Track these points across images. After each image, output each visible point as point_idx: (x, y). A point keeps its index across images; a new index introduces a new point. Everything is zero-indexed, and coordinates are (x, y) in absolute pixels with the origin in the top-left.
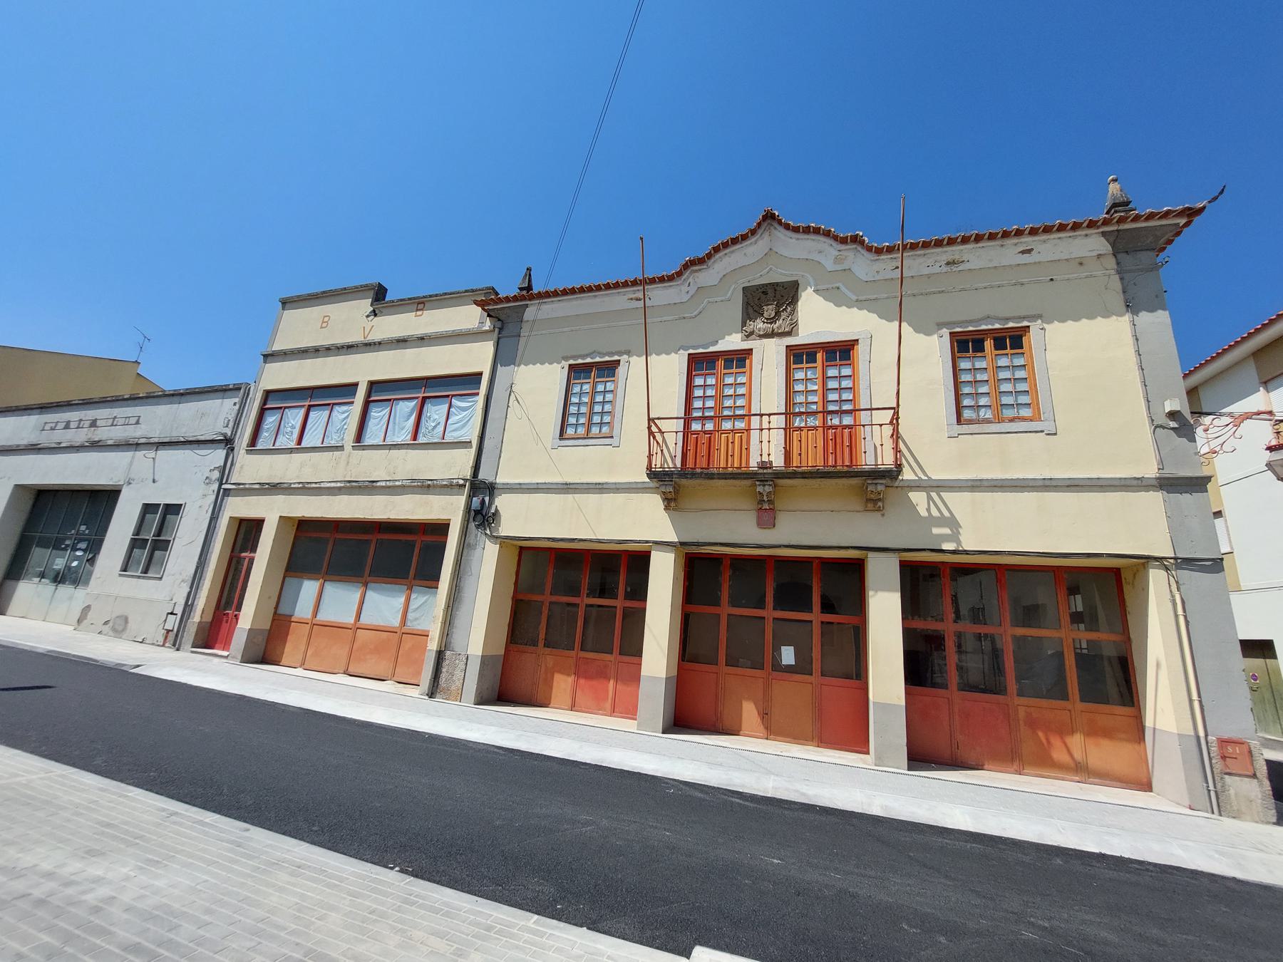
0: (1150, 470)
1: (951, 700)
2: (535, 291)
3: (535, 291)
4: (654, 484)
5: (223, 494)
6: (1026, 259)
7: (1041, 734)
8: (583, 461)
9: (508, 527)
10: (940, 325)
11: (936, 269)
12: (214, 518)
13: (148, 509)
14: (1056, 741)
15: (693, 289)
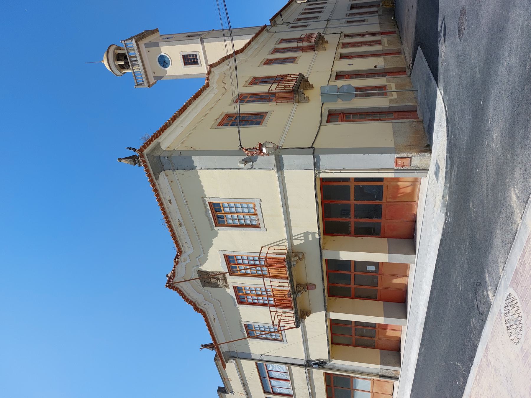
2: (212, 342)
3: (212, 342)
4: (301, 325)
6: (173, 201)
7: (399, 195)
9: (325, 356)
10: (212, 229)
11: (184, 229)
14: (402, 191)
15: (206, 303)
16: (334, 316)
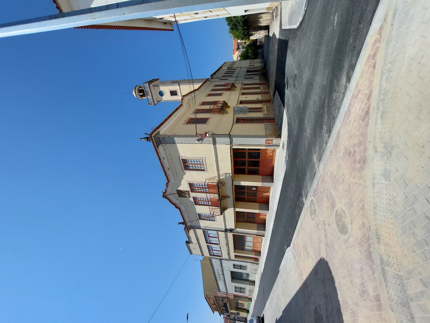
0: (212, 146)
1: (261, 168)
5: (230, 260)
6: (165, 158)
8: (210, 163)
9: (233, 227)
12: (235, 260)
13: (234, 268)
14: (268, 155)
15: (180, 204)
16: (237, 210)
